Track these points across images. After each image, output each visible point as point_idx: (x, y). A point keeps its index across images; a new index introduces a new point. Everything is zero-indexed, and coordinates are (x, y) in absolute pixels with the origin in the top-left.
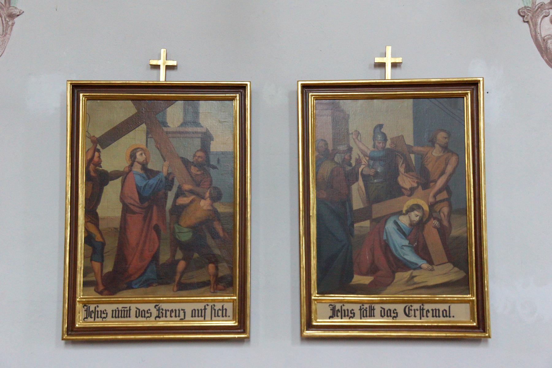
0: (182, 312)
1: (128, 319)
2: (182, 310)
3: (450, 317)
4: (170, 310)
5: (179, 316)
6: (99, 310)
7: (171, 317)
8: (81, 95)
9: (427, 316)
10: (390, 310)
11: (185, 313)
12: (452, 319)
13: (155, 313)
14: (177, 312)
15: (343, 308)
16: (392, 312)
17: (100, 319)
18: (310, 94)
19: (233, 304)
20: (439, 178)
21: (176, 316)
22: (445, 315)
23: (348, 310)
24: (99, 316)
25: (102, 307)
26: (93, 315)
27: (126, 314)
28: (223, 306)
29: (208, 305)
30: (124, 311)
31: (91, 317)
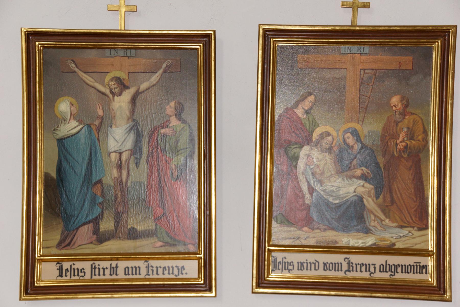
2: (372, 265)
6: (76, 268)
9: (361, 271)
11: (375, 268)
13: (345, 267)
14: (171, 269)
15: (73, 267)
18: (201, 45)
19: (199, 262)
22: (382, 270)
24: (76, 274)
28: (111, 265)
29: (74, 264)
30: (417, 266)
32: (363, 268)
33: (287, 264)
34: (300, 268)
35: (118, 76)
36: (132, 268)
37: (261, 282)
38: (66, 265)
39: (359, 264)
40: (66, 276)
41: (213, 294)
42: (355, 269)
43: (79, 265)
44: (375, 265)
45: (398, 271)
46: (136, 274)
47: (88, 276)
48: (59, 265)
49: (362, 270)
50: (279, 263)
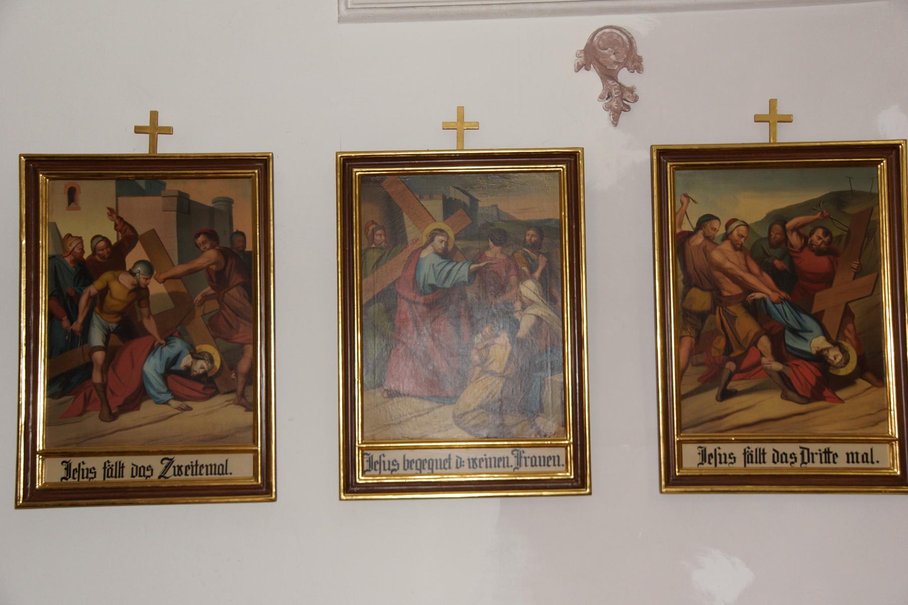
1: (763, 465)
3: (872, 463)
9: (201, 474)
10: (786, 455)
12: (229, 476)
13: (513, 461)
15: (718, 451)
20: (244, 389)
24: (723, 460)
26: (378, 467)
31: (375, 470)
36: (207, 466)
37: (350, 487)
38: (710, 448)
40: (201, 474)
41: (588, 490)
43: (726, 449)
47: (100, 477)
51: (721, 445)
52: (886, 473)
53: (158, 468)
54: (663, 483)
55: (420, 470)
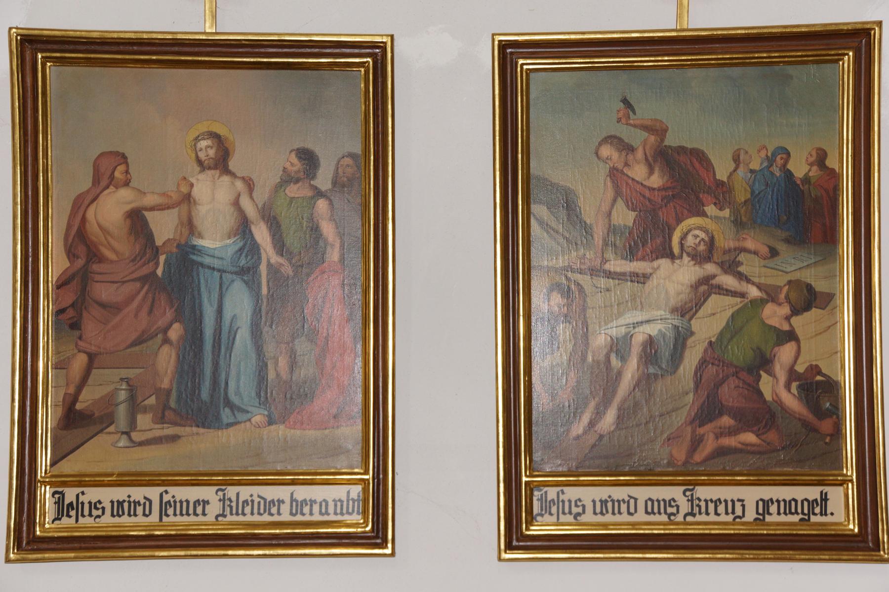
0: (738, 505)
2: (739, 500)
4: (318, 501)
5: (733, 513)
7: (717, 514)
8: (369, 60)
9: (244, 514)
11: (743, 506)
13: (685, 507)
16: (573, 504)
17: (570, 518)
21: (175, 515)
22: (649, 510)
23: (570, 501)
24: (86, 512)
25: (572, 493)
27: (118, 508)
28: (348, 492)
29: (83, 493)
31: (551, 514)
32: (721, 509)
33: (662, 503)
34: (115, 513)
35: (218, 132)
36: (778, 501)
37: (515, 537)
38: (70, 494)
39: (711, 501)
41: (388, 551)
42: (703, 509)
44: (742, 501)
45: (771, 511)
46: (188, 514)
48: (220, 493)
49: (719, 512)
50: (243, 502)
51: (566, 489)
52: (839, 530)
53: (214, 508)
54: (503, 547)
55: (763, 515)
